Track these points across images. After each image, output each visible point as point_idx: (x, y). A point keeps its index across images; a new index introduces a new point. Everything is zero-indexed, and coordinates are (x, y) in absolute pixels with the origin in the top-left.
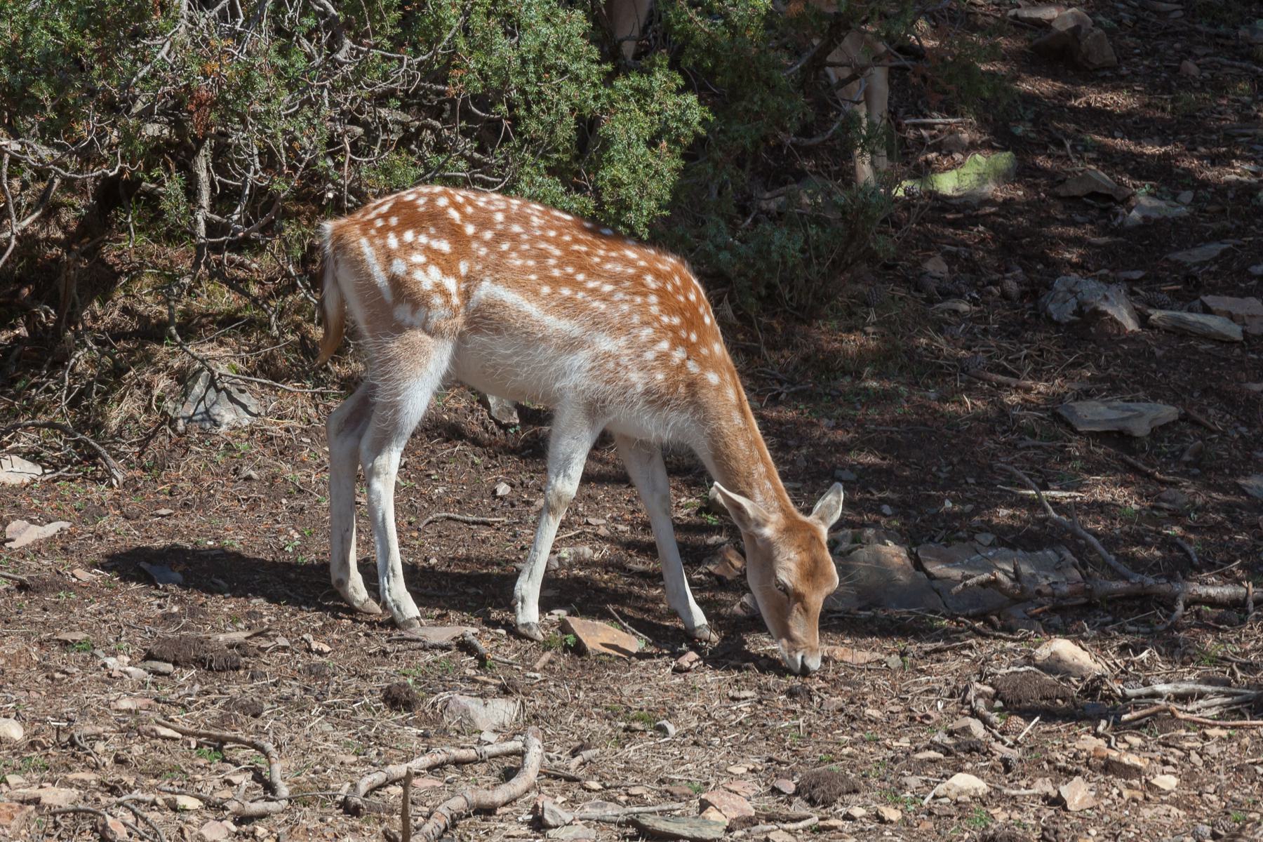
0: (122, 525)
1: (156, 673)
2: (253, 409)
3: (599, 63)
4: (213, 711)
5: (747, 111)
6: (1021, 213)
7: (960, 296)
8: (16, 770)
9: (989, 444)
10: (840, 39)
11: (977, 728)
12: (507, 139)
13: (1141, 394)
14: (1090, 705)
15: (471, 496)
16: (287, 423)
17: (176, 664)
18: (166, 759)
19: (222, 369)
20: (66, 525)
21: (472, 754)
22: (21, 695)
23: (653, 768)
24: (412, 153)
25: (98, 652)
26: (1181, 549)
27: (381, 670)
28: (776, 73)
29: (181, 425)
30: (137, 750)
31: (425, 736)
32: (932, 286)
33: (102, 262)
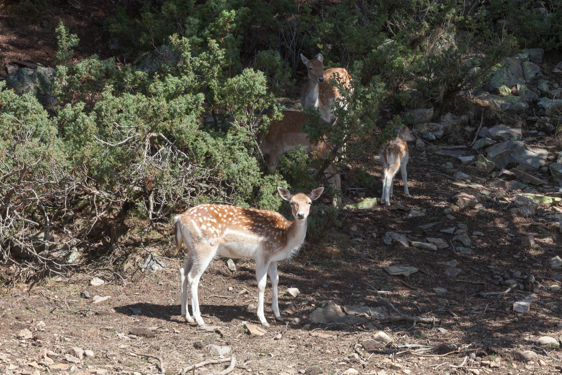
0: (125, 297)
1: (132, 338)
2: (163, 266)
3: (259, 172)
4: (146, 349)
5: (301, 186)
6: (379, 214)
7: (360, 237)
8: (91, 364)
9: (365, 278)
10: (327, 167)
11: (356, 355)
12: (234, 192)
13: (408, 265)
14: (389, 350)
15: (222, 290)
16: (172, 269)
17: (137, 335)
18: (132, 362)
19: (155, 254)
20: (110, 297)
21: (217, 361)
22: (94, 343)
23: (267, 366)
24: (209, 196)
25: (116, 332)
26: (416, 307)
27: (194, 338)
28: (309, 175)
29: (143, 270)
30: (124, 359)
31: (204, 356)
32: (352, 234)
33: (124, 225)
